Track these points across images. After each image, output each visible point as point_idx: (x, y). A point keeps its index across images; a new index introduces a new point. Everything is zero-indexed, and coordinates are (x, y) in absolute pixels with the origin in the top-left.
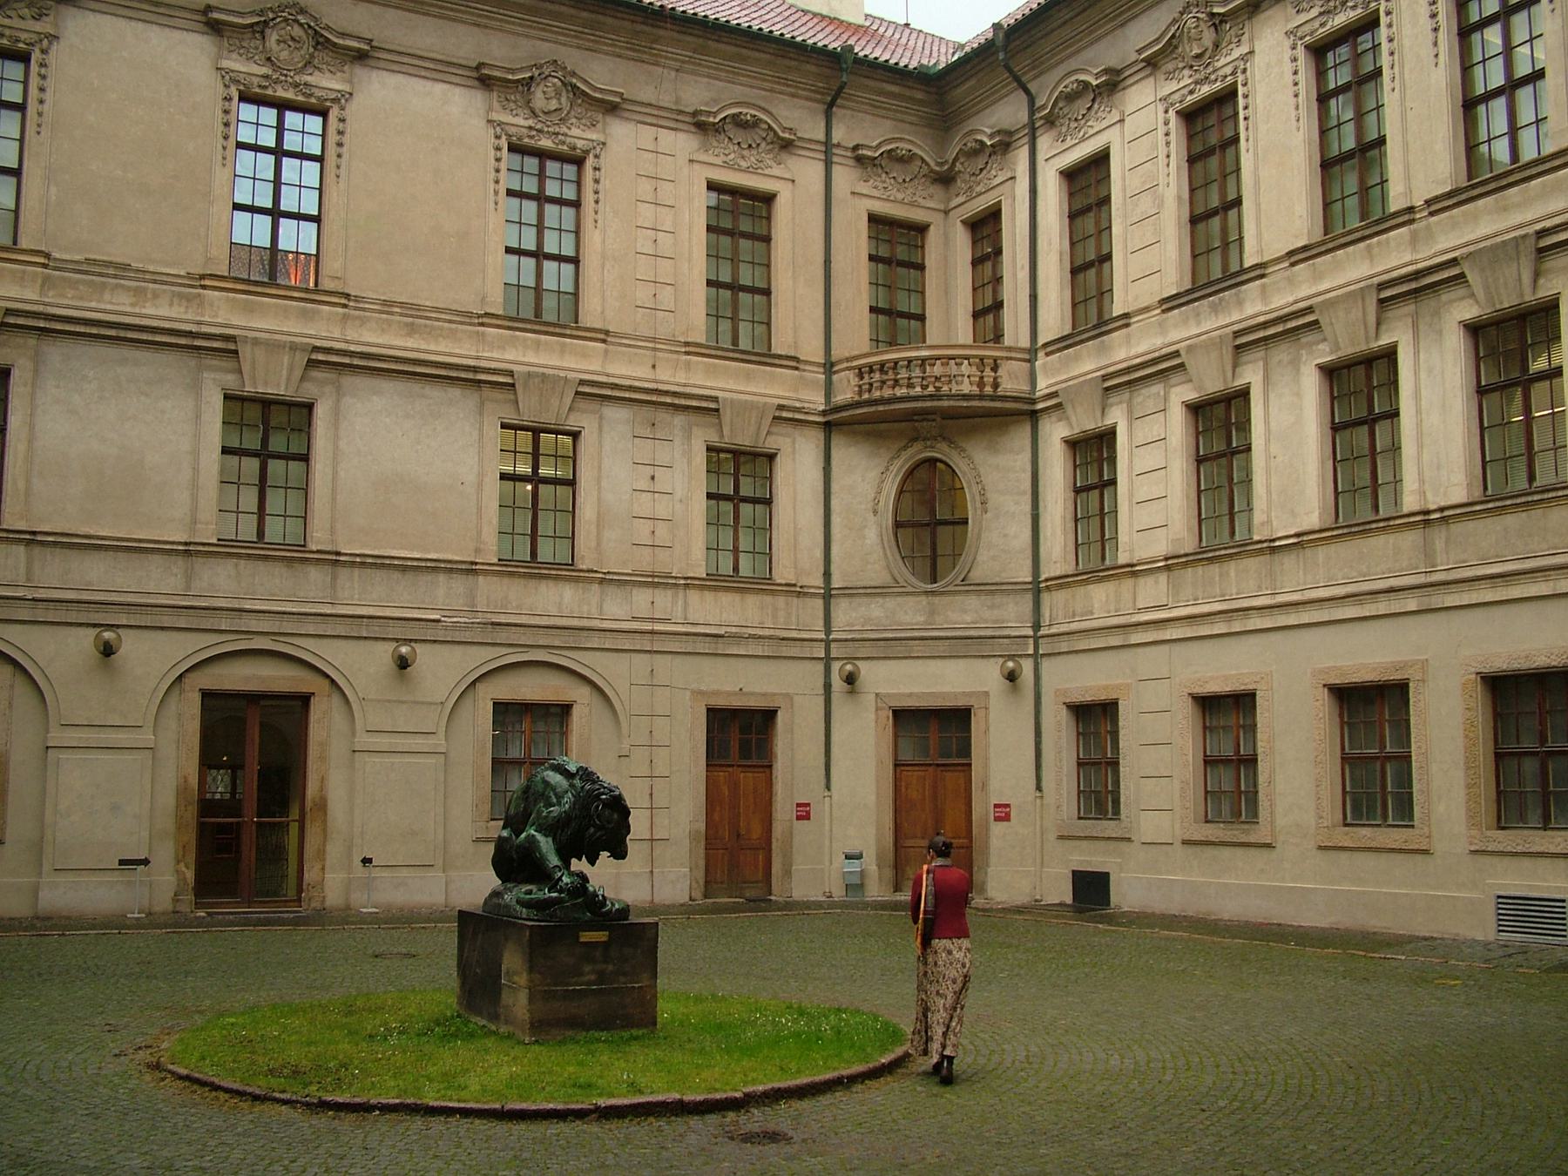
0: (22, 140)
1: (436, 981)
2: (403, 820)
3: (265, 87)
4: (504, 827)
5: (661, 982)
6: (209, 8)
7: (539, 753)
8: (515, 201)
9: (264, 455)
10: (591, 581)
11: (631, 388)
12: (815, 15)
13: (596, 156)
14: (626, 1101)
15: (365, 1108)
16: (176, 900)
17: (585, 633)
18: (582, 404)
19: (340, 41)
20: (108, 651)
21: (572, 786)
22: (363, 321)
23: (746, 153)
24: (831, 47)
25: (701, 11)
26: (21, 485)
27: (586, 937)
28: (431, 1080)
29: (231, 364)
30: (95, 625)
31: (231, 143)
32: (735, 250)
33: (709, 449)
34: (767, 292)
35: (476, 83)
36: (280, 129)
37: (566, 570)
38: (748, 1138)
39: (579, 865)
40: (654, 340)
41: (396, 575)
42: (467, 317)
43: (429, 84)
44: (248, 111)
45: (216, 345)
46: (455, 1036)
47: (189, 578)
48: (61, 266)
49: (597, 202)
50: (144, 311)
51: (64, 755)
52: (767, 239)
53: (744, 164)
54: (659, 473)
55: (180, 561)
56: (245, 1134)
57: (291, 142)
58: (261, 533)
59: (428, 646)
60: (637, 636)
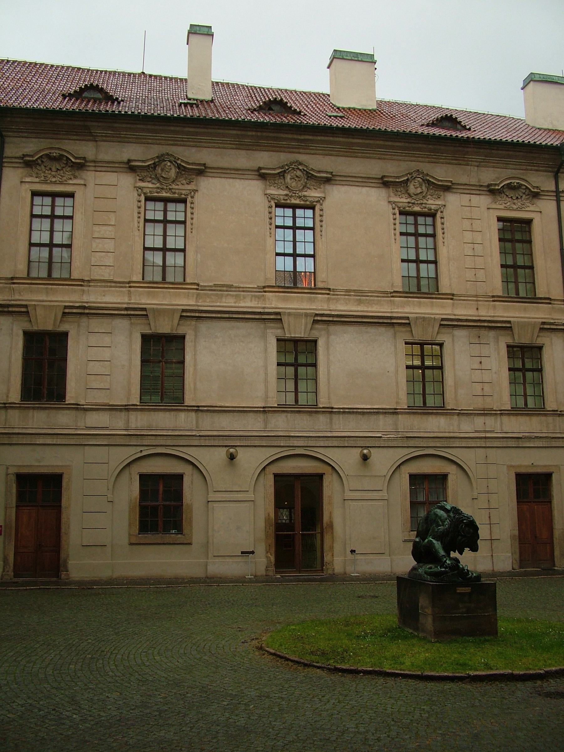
0: (185, 236)
1: (387, 611)
2: (369, 531)
3: (286, 200)
4: (417, 537)
5: (499, 612)
6: (260, 168)
7: (433, 498)
8: (404, 238)
9: (296, 365)
10: (453, 414)
11: (467, 320)
12: (545, 130)
13: (442, 212)
14: (484, 673)
15: (356, 672)
16: (267, 570)
17: (452, 440)
19: (318, 175)
20: (232, 457)
21: (449, 516)
22: (337, 300)
23: (515, 201)
24: (555, 144)
25: (487, 137)
26: (192, 386)
27: (460, 590)
28: (387, 659)
29: (279, 325)
30: (226, 446)
31: (273, 226)
32: (514, 249)
33: (508, 346)
34: (532, 268)
35: (382, 185)
36: (294, 217)
37: (441, 410)
38: (549, 695)
39: (453, 554)
40: (476, 296)
41: (360, 417)
42: (385, 294)
43: (360, 188)
45: (272, 317)
46: (398, 637)
47: (266, 422)
48: (204, 288)
49: (443, 233)
50: (240, 305)
51: (215, 505)
52: (530, 242)
53: (515, 207)
54: (483, 360)
55: (261, 416)
56: (301, 682)
57: (300, 222)
58: (297, 401)
59: (377, 449)
60: (478, 440)
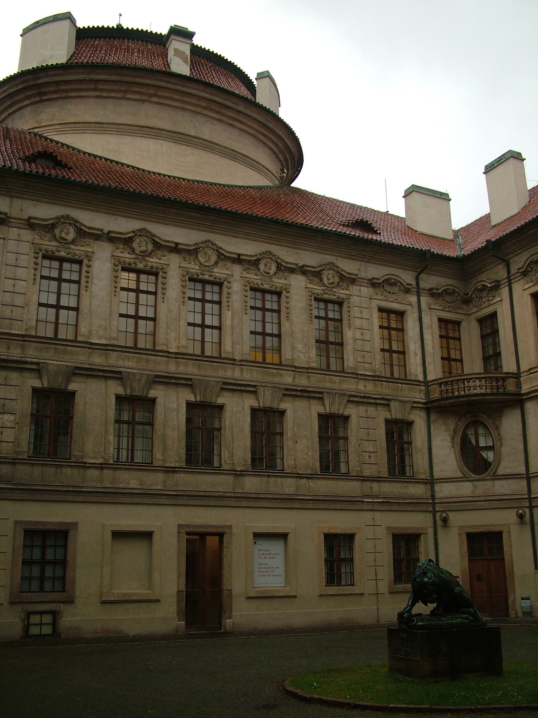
9: (131, 423)
18: (286, 399)
44: (125, 275)
59: (453, 512)
